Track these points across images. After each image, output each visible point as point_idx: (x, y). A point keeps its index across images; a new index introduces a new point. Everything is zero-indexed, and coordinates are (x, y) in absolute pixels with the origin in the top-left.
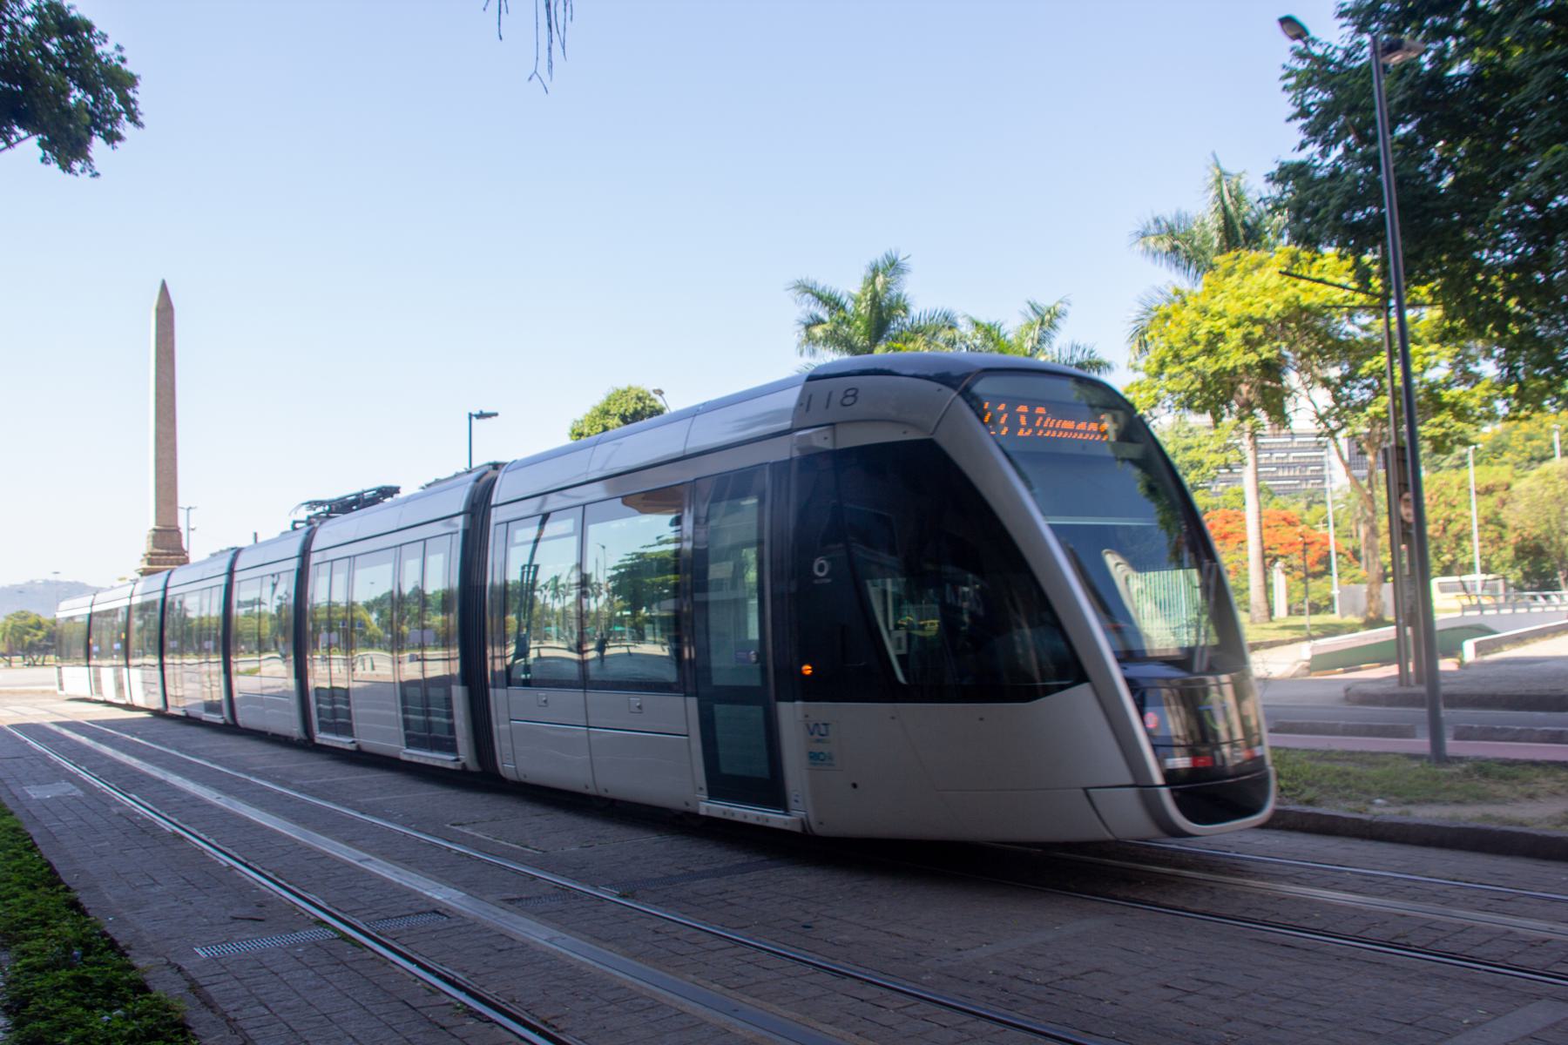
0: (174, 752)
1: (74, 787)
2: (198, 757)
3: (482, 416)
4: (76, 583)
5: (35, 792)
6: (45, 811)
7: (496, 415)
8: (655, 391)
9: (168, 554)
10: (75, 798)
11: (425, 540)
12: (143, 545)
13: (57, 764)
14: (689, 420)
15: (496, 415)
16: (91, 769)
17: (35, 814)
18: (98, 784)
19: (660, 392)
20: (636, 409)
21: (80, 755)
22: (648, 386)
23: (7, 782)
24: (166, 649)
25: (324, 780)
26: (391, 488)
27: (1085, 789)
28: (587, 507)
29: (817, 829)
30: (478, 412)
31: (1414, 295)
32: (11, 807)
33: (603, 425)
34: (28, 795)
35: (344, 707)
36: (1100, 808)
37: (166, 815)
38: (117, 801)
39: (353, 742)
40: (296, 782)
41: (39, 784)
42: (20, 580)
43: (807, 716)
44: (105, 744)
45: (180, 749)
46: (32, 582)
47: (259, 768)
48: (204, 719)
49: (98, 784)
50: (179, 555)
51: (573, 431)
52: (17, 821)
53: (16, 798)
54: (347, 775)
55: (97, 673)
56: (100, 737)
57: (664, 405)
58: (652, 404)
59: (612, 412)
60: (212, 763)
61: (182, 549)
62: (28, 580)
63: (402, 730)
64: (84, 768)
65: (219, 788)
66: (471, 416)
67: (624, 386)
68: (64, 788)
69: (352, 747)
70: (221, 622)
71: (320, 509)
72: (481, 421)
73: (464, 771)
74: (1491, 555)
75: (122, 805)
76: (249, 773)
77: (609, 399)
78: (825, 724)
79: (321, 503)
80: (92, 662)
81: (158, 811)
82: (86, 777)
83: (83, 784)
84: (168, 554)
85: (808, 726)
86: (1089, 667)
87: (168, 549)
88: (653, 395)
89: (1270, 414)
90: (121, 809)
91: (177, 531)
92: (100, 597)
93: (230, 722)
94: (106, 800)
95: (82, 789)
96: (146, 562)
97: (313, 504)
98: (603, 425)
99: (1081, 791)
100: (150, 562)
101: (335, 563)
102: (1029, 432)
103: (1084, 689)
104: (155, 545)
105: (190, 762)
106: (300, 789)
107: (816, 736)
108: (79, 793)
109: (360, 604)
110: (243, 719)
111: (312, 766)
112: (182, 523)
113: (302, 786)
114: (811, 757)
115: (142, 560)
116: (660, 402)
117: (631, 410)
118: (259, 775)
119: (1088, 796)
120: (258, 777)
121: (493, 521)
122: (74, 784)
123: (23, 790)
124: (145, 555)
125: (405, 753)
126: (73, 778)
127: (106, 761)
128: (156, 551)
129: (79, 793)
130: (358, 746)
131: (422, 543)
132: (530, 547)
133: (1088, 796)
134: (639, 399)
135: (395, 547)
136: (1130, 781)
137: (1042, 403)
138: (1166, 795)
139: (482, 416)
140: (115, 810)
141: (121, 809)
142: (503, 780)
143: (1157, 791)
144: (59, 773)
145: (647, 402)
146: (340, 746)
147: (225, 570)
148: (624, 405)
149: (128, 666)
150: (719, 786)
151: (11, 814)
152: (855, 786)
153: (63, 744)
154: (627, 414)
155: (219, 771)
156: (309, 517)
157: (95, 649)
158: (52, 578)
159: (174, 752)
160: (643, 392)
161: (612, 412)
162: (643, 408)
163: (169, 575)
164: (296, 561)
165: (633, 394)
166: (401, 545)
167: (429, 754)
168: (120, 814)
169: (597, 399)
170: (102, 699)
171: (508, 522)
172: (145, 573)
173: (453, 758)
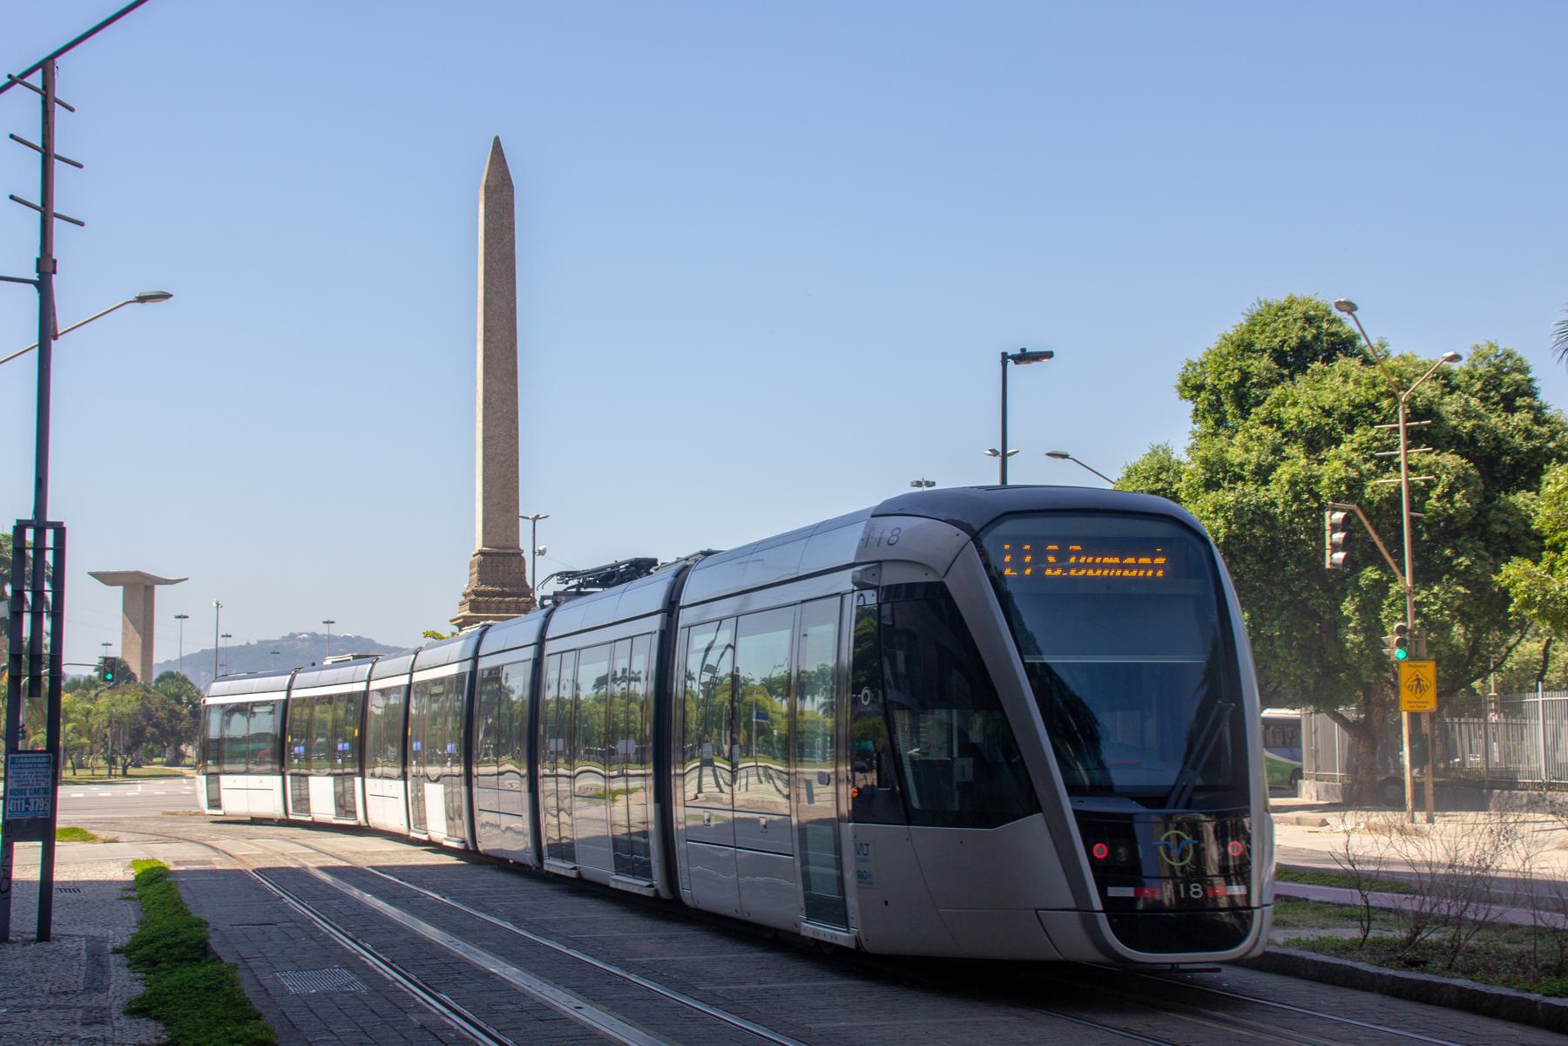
0: (508, 926)
1: (352, 978)
2: (548, 936)
3: (1024, 357)
4: (359, 638)
5: (294, 984)
6: (310, 1015)
7: (1049, 355)
8: (1339, 305)
9: (503, 594)
10: (354, 995)
11: (632, 637)
12: (463, 579)
13: (327, 937)
14: (804, 541)
15: (1049, 355)
16: (379, 949)
17: (294, 1019)
18: (390, 974)
19: (1350, 307)
20: (1302, 340)
21: (365, 924)
22: (1326, 296)
23: (252, 964)
24: (541, 752)
25: (753, 986)
26: (646, 560)
27: (1036, 910)
28: (740, 618)
29: (868, 947)
30: (1018, 352)
31: (1284, 477)
32: (258, 1005)
33: (1240, 370)
34: (283, 986)
35: (643, 840)
36: (1044, 923)
37: (494, 1032)
38: (417, 1005)
39: (575, 868)
40: (704, 987)
41: (300, 969)
42: (275, 633)
43: (855, 836)
44: (428, 921)
45: (516, 921)
46: (292, 636)
47: (644, 960)
48: (613, 885)
49: (390, 974)
50: (519, 596)
51: (1185, 384)
52: (265, 1028)
53: (266, 990)
54: (790, 980)
55: (419, 789)
56: (392, 897)
57: (1357, 331)
58: (1333, 329)
59: (1258, 346)
60: (569, 947)
61: (526, 585)
62: (286, 634)
63: (612, 851)
64: (368, 946)
65: (580, 991)
66: (1005, 357)
67: (1280, 298)
68: (337, 979)
69: (573, 874)
70: (527, 705)
71: (574, 582)
72: (1023, 366)
73: (657, 897)
74: (189, 757)
75: (427, 1011)
76: (628, 968)
77: (1252, 322)
78: (867, 845)
79: (574, 575)
80: (413, 769)
81: (483, 1025)
82: (371, 961)
83: (366, 973)
84: (503, 594)
85: (855, 845)
86: (1044, 802)
87: (503, 585)
88: (1336, 313)
89: (1469, 524)
90: (424, 1017)
91: (518, 554)
92: (381, 667)
93: (664, 894)
94: (402, 1004)
95: (365, 981)
96: (467, 606)
97: (565, 576)
98: (1240, 370)
99: (1033, 912)
100: (475, 606)
101: (634, 639)
102: (1058, 572)
103: (1038, 817)
104: (483, 579)
105: (535, 944)
106: (711, 999)
107: (862, 856)
108: (360, 987)
109: (757, 682)
110: (698, 889)
111: (731, 961)
112: (525, 544)
113: (714, 994)
114: (859, 876)
115: (461, 604)
116: (1349, 325)
117: (1293, 342)
118: (645, 972)
119: (1037, 914)
120: (643, 976)
121: (680, 624)
122: (353, 972)
123: (276, 978)
124: (465, 595)
125: (613, 880)
126: (352, 963)
127: (403, 937)
128: (483, 588)
129: (360, 987)
130: (579, 873)
131: (735, 619)
132: (703, 654)
133: (1037, 914)
134: (1309, 320)
135: (610, 643)
136: (1073, 905)
137: (1075, 541)
138: (1103, 921)
139: (1024, 357)
140: (415, 1019)
141: (424, 1017)
142: (687, 908)
143: (1095, 916)
144: (329, 954)
145: (1325, 325)
146: (636, 890)
147: (533, 638)
148: (1281, 333)
149: (362, 775)
150: (818, 908)
151: (258, 1017)
152: (886, 903)
153: (336, 904)
154: (1286, 348)
155: (581, 962)
156: (556, 594)
157: (416, 746)
158: (322, 630)
159: (508, 926)
160: (1316, 308)
161: (1258, 346)
162: (1316, 338)
163: (482, 634)
164: (658, 617)
165: (1298, 311)
166: (615, 641)
167: (562, 864)
168: (423, 1027)
169: (1230, 322)
170: (425, 838)
171: (689, 627)
172: (464, 622)
173: (648, 883)
